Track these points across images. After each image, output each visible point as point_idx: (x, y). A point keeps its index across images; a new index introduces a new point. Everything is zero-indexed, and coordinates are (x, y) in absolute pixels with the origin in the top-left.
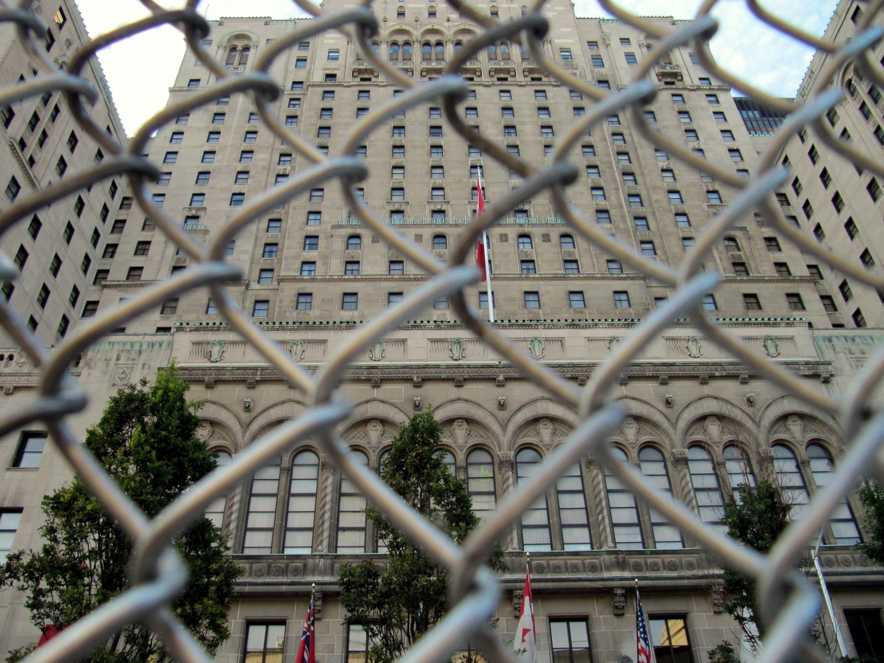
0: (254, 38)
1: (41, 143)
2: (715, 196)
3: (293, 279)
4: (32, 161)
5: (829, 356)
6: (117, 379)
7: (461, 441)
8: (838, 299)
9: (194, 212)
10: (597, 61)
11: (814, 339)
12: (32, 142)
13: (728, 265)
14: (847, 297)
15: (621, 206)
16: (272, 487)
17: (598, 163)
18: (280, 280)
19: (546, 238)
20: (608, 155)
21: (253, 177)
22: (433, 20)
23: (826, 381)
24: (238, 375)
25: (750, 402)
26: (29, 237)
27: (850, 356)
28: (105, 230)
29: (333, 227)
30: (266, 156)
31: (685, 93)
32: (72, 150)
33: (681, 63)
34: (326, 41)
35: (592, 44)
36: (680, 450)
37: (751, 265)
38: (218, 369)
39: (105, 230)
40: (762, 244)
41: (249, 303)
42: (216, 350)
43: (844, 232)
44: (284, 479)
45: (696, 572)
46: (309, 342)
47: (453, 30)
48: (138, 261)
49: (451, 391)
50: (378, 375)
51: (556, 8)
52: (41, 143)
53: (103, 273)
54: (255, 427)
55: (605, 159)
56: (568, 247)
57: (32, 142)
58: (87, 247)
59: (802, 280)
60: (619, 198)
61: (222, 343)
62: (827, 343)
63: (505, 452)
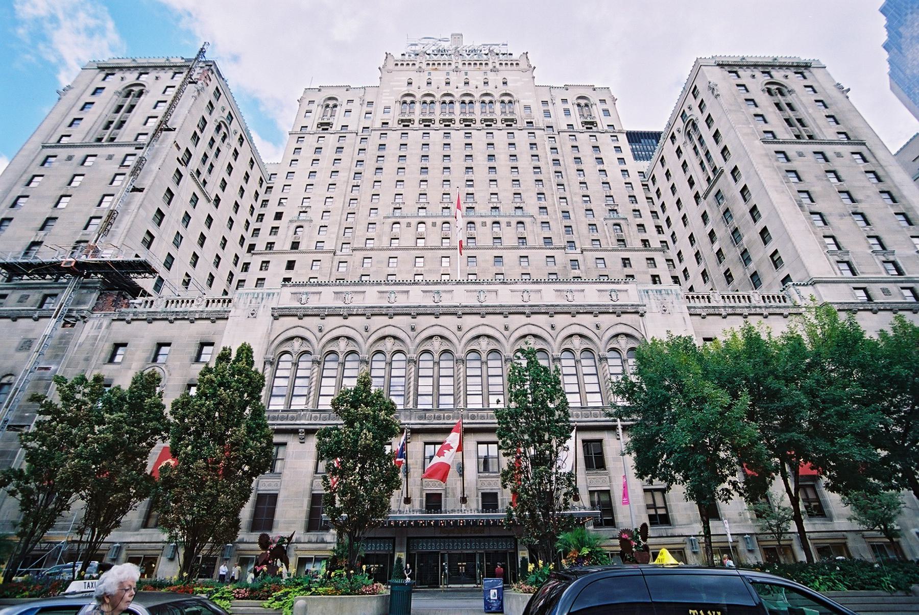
1: (210, 171)
3: (362, 249)
4: (205, 182)
5: (646, 301)
7: (437, 348)
8: (676, 261)
9: (304, 209)
10: (547, 114)
11: (640, 291)
12: (204, 170)
18: (354, 250)
19: (509, 224)
20: (549, 173)
23: (642, 315)
24: (316, 312)
25: (598, 327)
26: (206, 228)
28: (253, 220)
30: (347, 174)
31: (597, 134)
32: (230, 174)
33: (597, 116)
35: (545, 103)
36: (556, 354)
37: (628, 241)
38: (304, 308)
39: (248, 235)
40: (636, 228)
41: (336, 263)
42: (304, 297)
46: (356, 292)
48: (271, 239)
49: (431, 320)
50: (391, 311)
52: (210, 171)
53: (252, 247)
54: (324, 340)
56: (521, 229)
57: (204, 170)
59: (656, 250)
63: (460, 354)
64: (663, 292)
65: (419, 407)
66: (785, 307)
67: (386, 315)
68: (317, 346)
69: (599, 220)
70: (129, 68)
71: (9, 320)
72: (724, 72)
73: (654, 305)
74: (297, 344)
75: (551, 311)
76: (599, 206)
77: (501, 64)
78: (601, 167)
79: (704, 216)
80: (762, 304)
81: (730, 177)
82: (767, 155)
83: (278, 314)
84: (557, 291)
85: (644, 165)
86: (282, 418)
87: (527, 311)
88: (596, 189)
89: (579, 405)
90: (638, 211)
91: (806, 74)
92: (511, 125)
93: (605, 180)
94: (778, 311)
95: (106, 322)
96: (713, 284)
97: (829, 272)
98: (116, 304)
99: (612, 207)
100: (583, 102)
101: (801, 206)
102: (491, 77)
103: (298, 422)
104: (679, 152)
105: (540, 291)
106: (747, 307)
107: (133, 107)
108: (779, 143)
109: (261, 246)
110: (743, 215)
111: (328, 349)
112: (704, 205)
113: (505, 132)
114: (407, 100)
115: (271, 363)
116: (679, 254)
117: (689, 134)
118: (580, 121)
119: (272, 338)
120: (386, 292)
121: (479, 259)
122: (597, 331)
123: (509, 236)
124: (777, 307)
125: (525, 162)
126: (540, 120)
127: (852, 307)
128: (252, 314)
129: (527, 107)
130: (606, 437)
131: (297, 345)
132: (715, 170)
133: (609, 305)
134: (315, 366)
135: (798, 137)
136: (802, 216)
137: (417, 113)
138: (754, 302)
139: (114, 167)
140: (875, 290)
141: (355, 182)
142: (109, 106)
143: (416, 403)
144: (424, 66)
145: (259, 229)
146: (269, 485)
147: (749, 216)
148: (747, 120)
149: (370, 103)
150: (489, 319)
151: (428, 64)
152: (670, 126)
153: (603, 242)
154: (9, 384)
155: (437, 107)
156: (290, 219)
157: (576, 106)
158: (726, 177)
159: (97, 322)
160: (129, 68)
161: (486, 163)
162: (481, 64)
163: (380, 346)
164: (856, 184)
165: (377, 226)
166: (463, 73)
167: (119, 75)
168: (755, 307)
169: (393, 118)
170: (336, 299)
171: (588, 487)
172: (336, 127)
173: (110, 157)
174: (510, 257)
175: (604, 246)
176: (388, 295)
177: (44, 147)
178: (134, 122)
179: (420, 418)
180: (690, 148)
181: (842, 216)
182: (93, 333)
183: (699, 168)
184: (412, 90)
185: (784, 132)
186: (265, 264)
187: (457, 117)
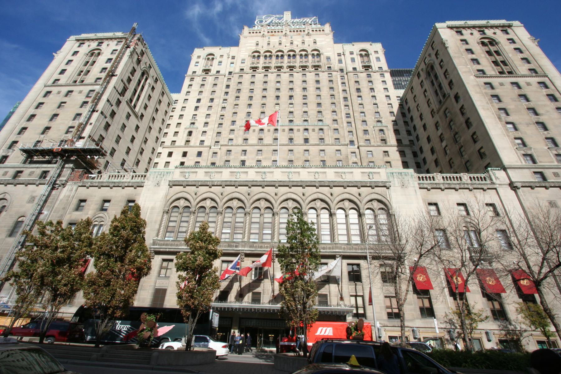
2: (378, 114)
3: (226, 145)
5: (391, 179)
10: (340, 61)
13: (379, 140)
15: (342, 118)
17: (335, 102)
18: (221, 146)
20: (339, 99)
22: (280, 46)
24: (193, 183)
29: (240, 126)
30: (218, 100)
31: (372, 74)
35: (339, 55)
37: (388, 140)
38: (187, 181)
42: (187, 175)
45: (331, 250)
46: (217, 172)
47: (287, 50)
50: (237, 184)
55: (338, 100)
56: (321, 134)
58: (157, 134)
59: (406, 146)
60: (341, 115)
61: (189, 173)
64: (403, 174)
65: (251, 240)
66: (484, 184)
67: (234, 186)
68: (194, 203)
69: (370, 128)
70: (93, 40)
71: (24, 185)
72: (453, 32)
73: (396, 182)
75: (331, 185)
76: (371, 119)
77: (313, 31)
78: (373, 94)
79: (437, 125)
80: (469, 181)
81: (453, 100)
82: (478, 85)
83: (173, 184)
84: (336, 172)
86: (171, 245)
87: (317, 185)
88: (369, 108)
89: (346, 242)
91: (509, 30)
92: (317, 69)
93: (389, 102)
94: (480, 186)
95: (75, 187)
96: (442, 168)
97: (517, 162)
98: (81, 177)
99: (379, 119)
100: (363, 53)
101: (500, 118)
102: (307, 39)
103: (180, 247)
105: (352, 172)
106: (458, 184)
107: (94, 62)
108: (487, 77)
109: (168, 142)
110: (462, 124)
111: (200, 205)
112: (437, 118)
113: (326, 73)
114: (256, 55)
118: (361, 65)
119: (168, 198)
120: (235, 172)
121: (295, 151)
122: (303, 197)
123: (299, 137)
124: (479, 184)
125: (325, 92)
126: (336, 66)
127: (532, 184)
129: (328, 58)
130: (362, 262)
132: (444, 96)
133: (367, 182)
134: (192, 215)
135: (500, 73)
136: (500, 125)
137: (261, 62)
138: (463, 180)
139: (83, 98)
140: (548, 173)
141: (223, 105)
142: (81, 62)
143: (249, 238)
144: (266, 33)
145: (178, 132)
146: (163, 283)
147: (464, 125)
148: (466, 63)
149: (233, 58)
150: (294, 189)
151: (290, 31)
152: (417, 67)
153: (372, 141)
154: (22, 222)
155: (262, 59)
156: (185, 127)
157: (359, 56)
158: (451, 100)
159: (70, 187)
160: (93, 40)
161: (301, 93)
162: (301, 31)
163: (256, 204)
164: (540, 103)
165: (235, 132)
166: (290, 37)
167: (87, 43)
168: (464, 184)
169: (247, 66)
170: (206, 176)
171: (349, 293)
172: (213, 72)
173: (81, 92)
174: (314, 150)
175: (372, 144)
176: (235, 174)
177: (45, 86)
178: (95, 72)
179: (250, 247)
181: (528, 125)
182: (68, 194)
184: (259, 48)
185: (490, 69)
186: (170, 154)
187: (285, 65)
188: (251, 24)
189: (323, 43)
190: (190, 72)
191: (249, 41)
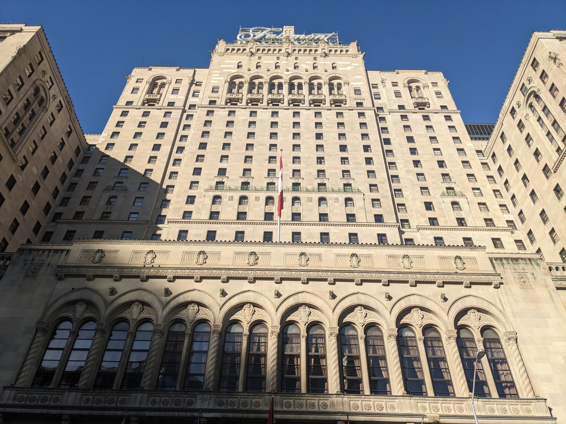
0: (169, 78)
6: (30, 272)
14: (532, 241)
16: (121, 345)
21: (160, 159)
27: (514, 271)
34: (212, 82)
43: (529, 199)
44: (129, 340)
51: (353, 64)
62: (532, 275)
74: (80, 309)
85: (482, 145)
90: (478, 189)
104: (521, 125)
115: (44, 331)
116: (530, 233)
117: (531, 106)
128: (33, 273)
131: (80, 311)
180: (533, 119)
183: (546, 140)
184: (241, 72)
188: (231, 39)
189: (349, 68)
190: (122, 102)
191: (226, 62)
